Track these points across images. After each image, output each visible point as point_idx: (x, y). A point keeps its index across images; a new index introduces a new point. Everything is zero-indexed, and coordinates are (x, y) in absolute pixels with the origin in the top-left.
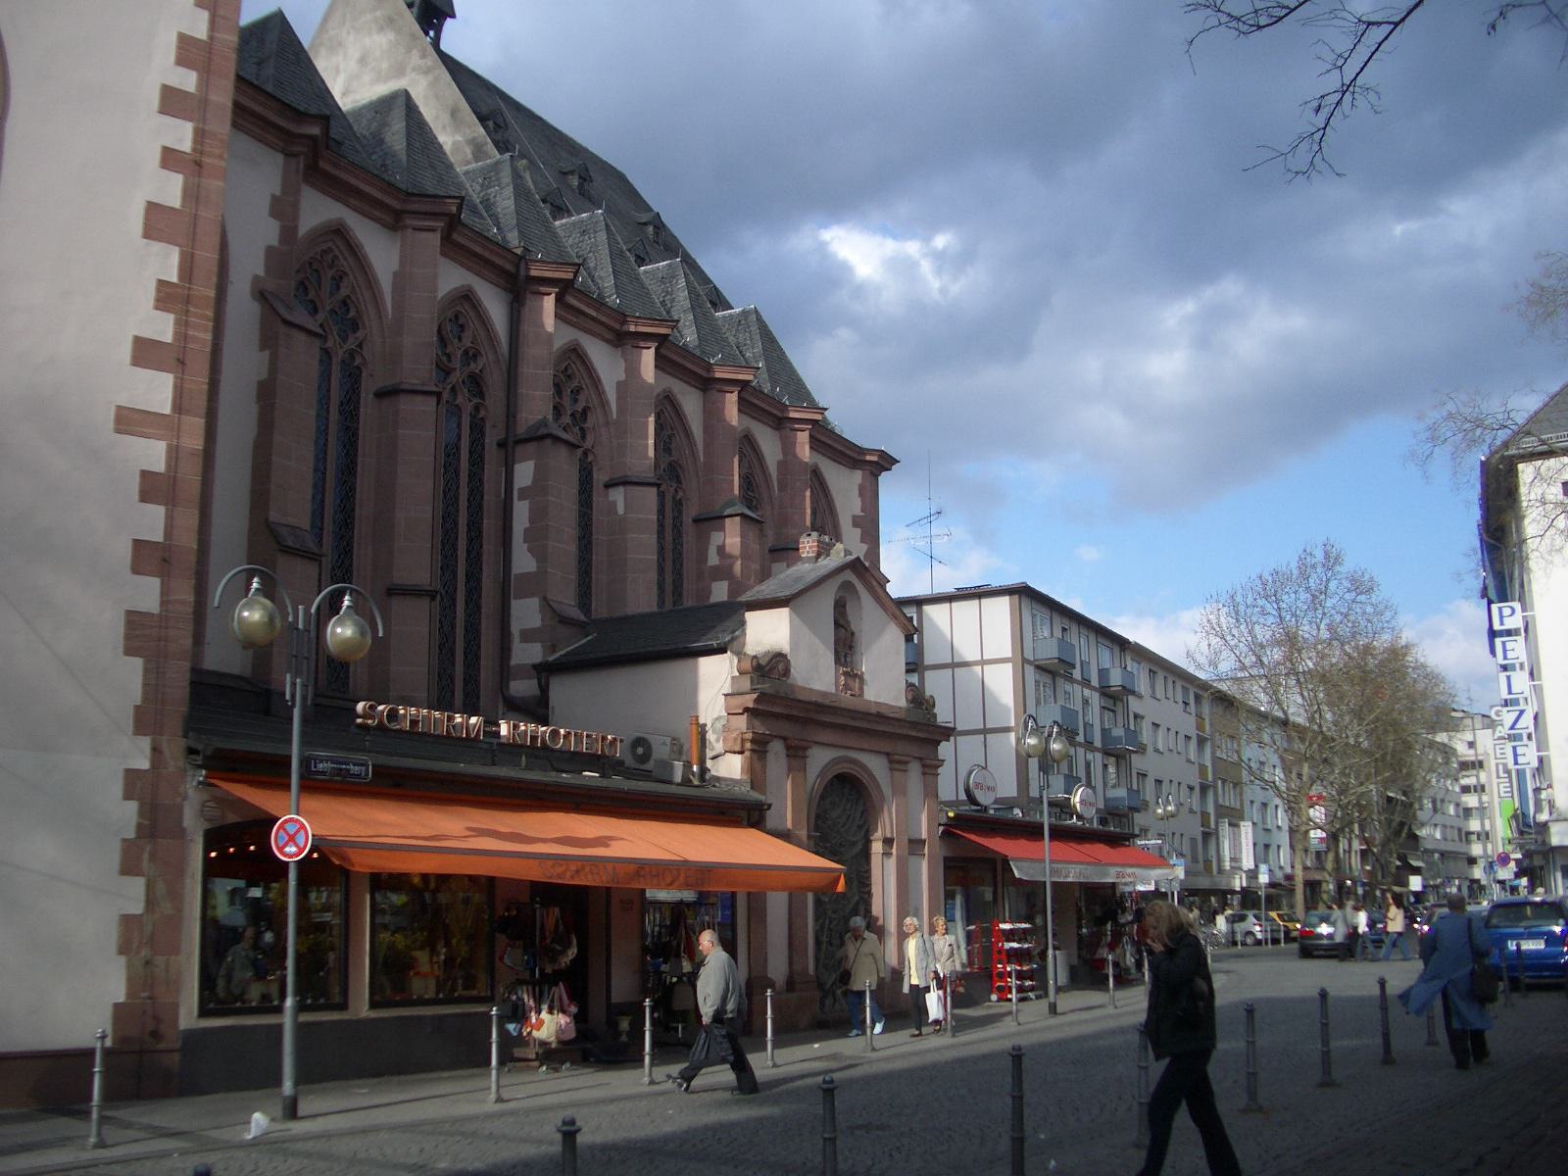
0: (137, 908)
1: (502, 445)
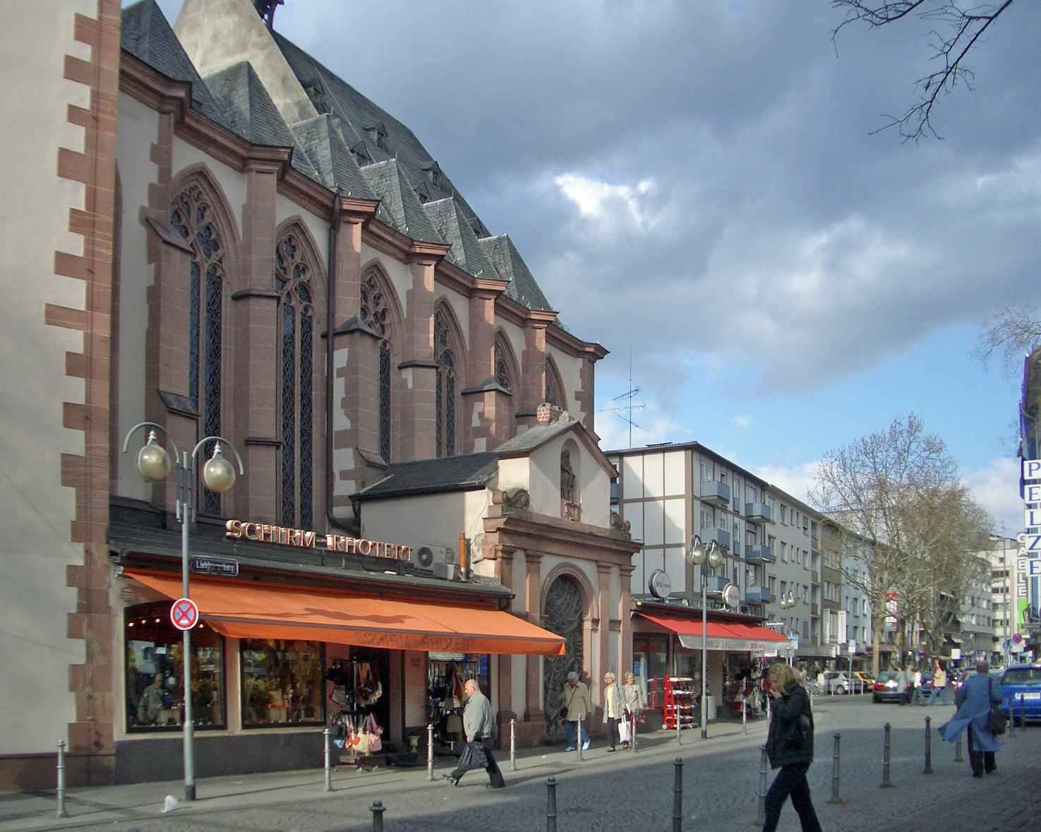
0: (82, 660)
1: (324, 336)
